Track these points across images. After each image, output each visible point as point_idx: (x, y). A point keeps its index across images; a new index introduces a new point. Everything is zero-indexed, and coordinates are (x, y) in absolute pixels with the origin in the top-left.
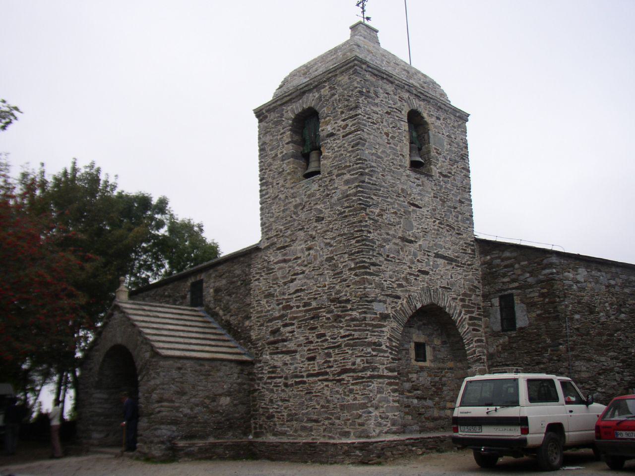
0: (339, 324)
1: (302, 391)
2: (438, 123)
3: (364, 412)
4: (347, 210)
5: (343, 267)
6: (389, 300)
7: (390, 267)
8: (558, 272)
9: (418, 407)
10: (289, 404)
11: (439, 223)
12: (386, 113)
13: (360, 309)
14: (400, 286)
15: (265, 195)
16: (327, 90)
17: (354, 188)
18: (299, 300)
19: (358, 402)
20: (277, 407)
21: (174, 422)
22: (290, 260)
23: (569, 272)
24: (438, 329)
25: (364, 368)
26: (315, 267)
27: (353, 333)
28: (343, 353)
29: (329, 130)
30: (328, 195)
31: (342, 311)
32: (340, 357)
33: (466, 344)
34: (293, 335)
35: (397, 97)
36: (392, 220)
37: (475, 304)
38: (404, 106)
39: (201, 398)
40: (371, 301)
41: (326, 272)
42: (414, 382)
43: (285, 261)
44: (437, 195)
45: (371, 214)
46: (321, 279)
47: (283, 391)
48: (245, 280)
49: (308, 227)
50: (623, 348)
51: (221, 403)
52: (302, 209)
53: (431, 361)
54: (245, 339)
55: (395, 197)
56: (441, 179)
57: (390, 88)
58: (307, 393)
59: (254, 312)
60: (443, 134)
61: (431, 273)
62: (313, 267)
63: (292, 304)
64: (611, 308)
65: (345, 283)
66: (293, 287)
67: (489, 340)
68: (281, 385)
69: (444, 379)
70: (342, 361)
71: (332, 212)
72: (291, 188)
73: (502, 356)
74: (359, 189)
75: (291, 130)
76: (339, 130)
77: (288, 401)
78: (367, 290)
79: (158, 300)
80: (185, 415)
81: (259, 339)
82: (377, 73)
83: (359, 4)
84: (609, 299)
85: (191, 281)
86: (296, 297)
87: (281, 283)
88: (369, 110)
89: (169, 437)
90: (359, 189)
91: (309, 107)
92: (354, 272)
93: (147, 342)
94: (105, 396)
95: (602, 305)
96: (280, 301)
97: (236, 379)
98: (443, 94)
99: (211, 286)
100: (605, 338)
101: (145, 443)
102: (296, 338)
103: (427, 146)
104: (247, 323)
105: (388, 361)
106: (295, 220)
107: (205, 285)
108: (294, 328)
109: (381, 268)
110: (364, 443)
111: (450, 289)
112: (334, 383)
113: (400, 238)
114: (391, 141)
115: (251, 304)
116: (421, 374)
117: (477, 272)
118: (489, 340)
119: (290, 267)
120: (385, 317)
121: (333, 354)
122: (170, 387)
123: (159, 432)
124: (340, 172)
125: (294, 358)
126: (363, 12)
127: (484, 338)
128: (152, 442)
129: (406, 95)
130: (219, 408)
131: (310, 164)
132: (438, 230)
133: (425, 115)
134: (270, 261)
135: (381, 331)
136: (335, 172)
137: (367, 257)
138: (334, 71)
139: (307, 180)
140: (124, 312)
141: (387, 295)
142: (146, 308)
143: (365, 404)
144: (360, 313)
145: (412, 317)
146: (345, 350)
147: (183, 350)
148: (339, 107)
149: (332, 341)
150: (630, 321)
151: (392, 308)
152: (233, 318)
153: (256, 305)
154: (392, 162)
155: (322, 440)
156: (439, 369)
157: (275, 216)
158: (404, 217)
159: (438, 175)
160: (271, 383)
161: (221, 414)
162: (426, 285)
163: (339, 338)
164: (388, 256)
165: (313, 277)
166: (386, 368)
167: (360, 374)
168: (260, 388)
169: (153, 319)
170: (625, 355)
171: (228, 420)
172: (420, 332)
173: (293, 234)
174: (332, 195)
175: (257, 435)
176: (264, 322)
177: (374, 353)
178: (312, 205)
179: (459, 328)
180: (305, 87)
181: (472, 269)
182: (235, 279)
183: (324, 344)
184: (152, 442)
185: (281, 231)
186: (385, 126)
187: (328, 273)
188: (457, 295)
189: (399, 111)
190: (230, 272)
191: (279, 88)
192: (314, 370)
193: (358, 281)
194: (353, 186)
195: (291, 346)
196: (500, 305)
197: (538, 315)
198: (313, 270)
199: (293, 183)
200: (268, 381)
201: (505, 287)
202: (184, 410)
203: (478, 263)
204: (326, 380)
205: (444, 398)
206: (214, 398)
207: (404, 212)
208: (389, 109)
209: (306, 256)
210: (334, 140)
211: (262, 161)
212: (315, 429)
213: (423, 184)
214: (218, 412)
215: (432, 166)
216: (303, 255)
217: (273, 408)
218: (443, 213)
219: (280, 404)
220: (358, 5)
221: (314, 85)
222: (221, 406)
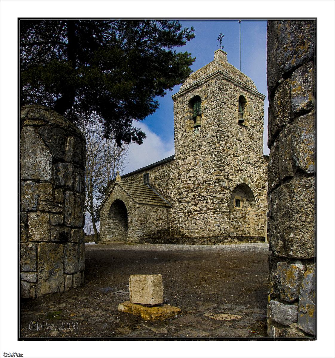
1: (191, 218)
3: (216, 225)
14: (232, 175)
19: (214, 221)
22: (187, 164)
25: (217, 208)
30: (204, 136)
41: (202, 169)
43: (185, 164)
45: (221, 144)
52: (193, 142)
57: (232, 86)
58: (193, 218)
60: (253, 107)
66: (188, 175)
69: (246, 215)
72: (188, 133)
75: (188, 106)
83: (219, 39)
111: (251, 177)
113: (232, 155)
116: (237, 212)
120: (225, 188)
126: (221, 43)
127: (264, 199)
129: (238, 89)
133: (246, 98)
145: (235, 188)
159: (250, 126)
167: (215, 210)
177: (221, 202)
194: (215, 132)
195: (187, 200)
220: (218, 40)
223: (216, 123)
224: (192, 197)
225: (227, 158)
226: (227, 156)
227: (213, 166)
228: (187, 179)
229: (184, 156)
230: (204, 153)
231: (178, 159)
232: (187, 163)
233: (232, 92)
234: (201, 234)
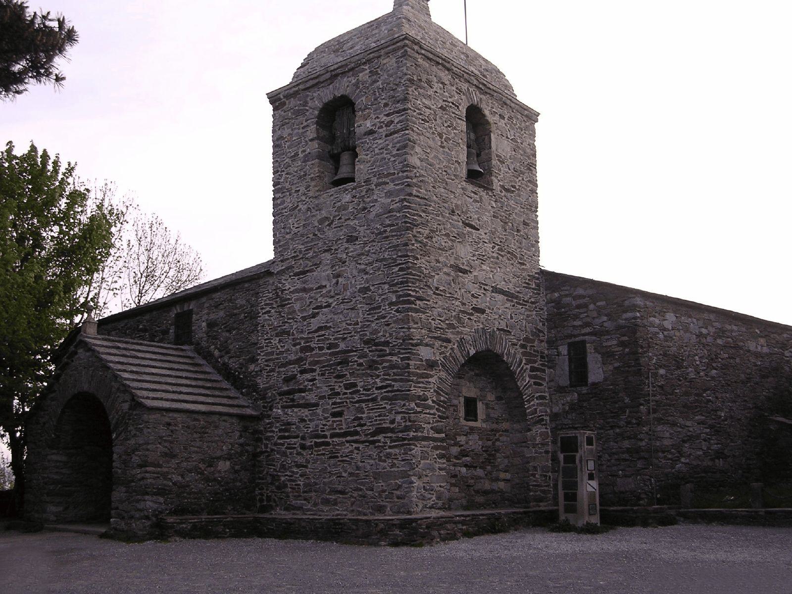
0: (374, 372)
1: (324, 454)
2: (502, 123)
4: (388, 229)
5: (382, 300)
6: (438, 343)
7: (440, 303)
8: (642, 316)
10: (307, 470)
11: (499, 250)
12: (440, 108)
13: (403, 354)
14: (451, 326)
15: (280, 205)
16: (366, 74)
18: (323, 340)
19: (396, 469)
20: (290, 474)
21: (161, 492)
23: (655, 317)
24: (492, 381)
26: (345, 299)
28: (379, 408)
29: (367, 126)
31: (379, 356)
33: (526, 401)
34: (314, 384)
35: (454, 88)
36: (443, 244)
37: (538, 352)
38: (462, 99)
40: (417, 345)
42: (462, 446)
43: (304, 290)
44: (497, 213)
46: (352, 314)
47: (298, 454)
49: (337, 247)
50: (712, 410)
51: (219, 468)
52: (329, 225)
53: (484, 421)
54: (248, 387)
55: (447, 215)
56: (503, 194)
57: (446, 77)
58: (331, 457)
59: (262, 354)
61: (488, 311)
62: (343, 300)
63: (313, 345)
64: (701, 362)
65: (384, 320)
66: (315, 323)
67: (553, 397)
69: (498, 443)
70: (378, 418)
71: (368, 231)
73: (569, 417)
74: (405, 203)
76: (382, 127)
77: (306, 467)
78: (411, 330)
79: (129, 335)
81: (270, 388)
82: (431, 56)
84: (699, 351)
85: (175, 312)
87: (299, 317)
88: (421, 103)
89: (155, 510)
90: (405, 203)
91: (342, 96)
93: (126, 389)
94: (64, 459)
95: (690, 358)
96: (298, 341)
98: (509, 87)
100: (692, 398)
101: (123, 518)
102: (318, 388)
104: (252, 367)
105: (434, 420)
106: (319, 239)
108: (315, 376)
110: (405, 519)
111: (508, 331)
112: (366, 445)
113: (451, 266)
115: (258, 343)
117: (541, 312)
118: (553, 397)
120: (431, 365)
121: (366, 410)
122: (157, 448)
123: (141, 506)
124: (380, 180)
125: (315, 413)
127: (546, 394)
128: (132, 517)
129: (464, 86)
130: (217, 475)
131: (340, 168)
132: (498, 258)
133: (487, 112)
134: (285, 290)
135: (427, 382)
136: (375, 180)
137: (413, 289)
138: (377, 51)
139: (336, 188)
140: (94, 351)
141: (435, 338)
142: (119, 345)
143: (406, 471)
144: (402, 359)
146: (382, 405)
147: (173, 400)
148: (383, 97)
149: (364, 392)
150: (721, 379)
151: (440, 354)
152: (232, 360)
154: (445, 171)
155: (350, 516)
156: (492, 430)
157: (293, 233)
158: (457, 240)
160: (283, 445)
161: (219, 483)
162: (481, 326)
163: (374, 389)
165: (342, 312)
166: (432, 428)
167: (400, 435)
168: (269, 450)
169: (131, 361)
170: (714, 419)
171: (227, 490)
172: (472, 384)
173: (316, 256)
174: (369, 209)
175: (264, 509)
176: (275, 367)
177: (419, 409)
178: (343, 220)
179: (518, 381)
180: (338, 68)
181: (536, 307)
183: (355, 396)
184: (132, 517)
185: (300, 252)
186: (438, 125)
187: (362, 307)
188: (517, 340)
189: (456, 106)
190: (230, 301)
191: (301, 67)
192: (340, 429)
193: (400, 319)
194: (397, 199)
195: (311, 398)
196: (569, 354)
197: (615, 368)
198: (341, 303)
199: (317, 191)
200: (279, 441)
201: (576, 332)
203: (544, 300)
204: (356, 442)
205: (498, 466)
206: (211, 462)
208: (444, 103)
209: (334, 285)
210: (374, 139)
211: (277, 161)
212: (340, 503)
213: (481, 199)
214: (215, 480)
216: (329, 284)
218: (504, 237)
219: (295, 470)
221: (349, 67)
222: (219, 472)
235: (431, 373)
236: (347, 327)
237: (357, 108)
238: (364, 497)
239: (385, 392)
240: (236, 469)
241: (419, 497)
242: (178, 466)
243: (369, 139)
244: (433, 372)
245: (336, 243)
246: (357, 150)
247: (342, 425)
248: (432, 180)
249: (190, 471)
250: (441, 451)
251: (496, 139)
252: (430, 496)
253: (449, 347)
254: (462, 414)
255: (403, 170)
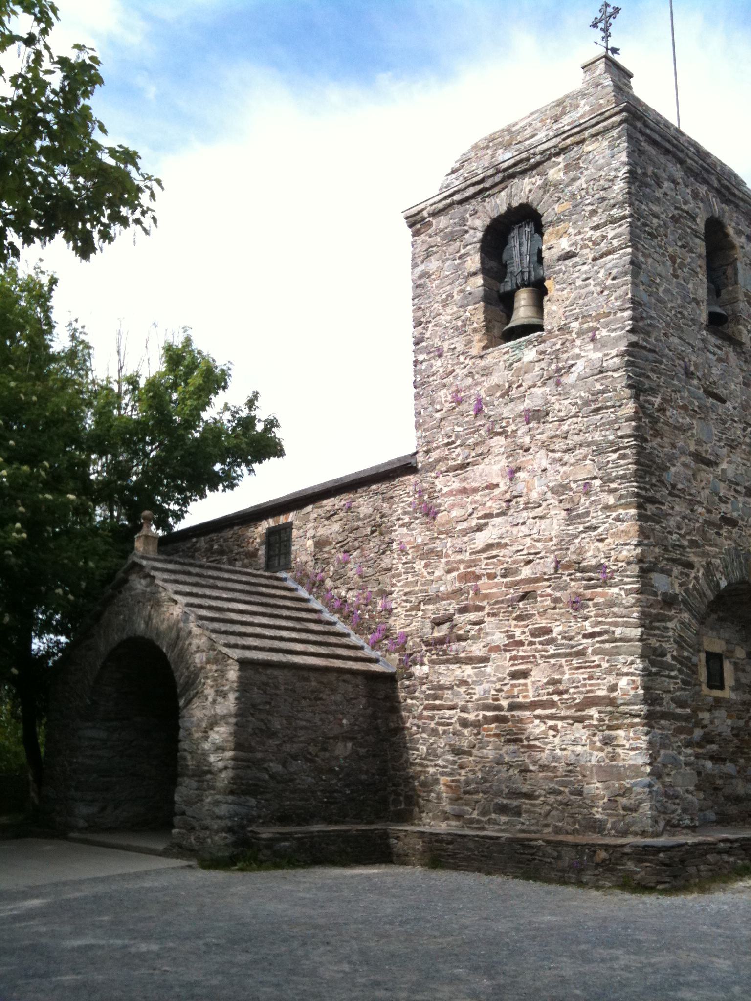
6: (676, 570)
9: (714, 776)
10: (471, 758)
14: (693, 544)
17: (617, 356)
22: (475, 490)
27: (613, 628)
32: (583, 673)
34: (480, 629)
35: (689, 191)
36: (680, 420)
39: (301, 742)
43: (464, 491)
48: (380, 526)
51: (337, 752)
53: (734, 689)
59: (399, 584)
61: (741, 523)
62: (526, 504)
63: (478, 571)
66: (481, 539)
68: (452, 721)
70: (587, 682)
76: (586, 247)
80: (272, 777)
86: (488, 558)
92: (614, 514)
96: (455, 565)
97: (364, 709)
99: (308, 535)
103: (731, 289)
107: (295, 533)
109: (663, 508)
112: (568, 724)
113: (691, 454)
114: (679, 272)
116: (717, 713)
119: (475, 502)
129: (703, 189)
133: (731, 231)
149: (564, 641)
152: (351, 593)
153: (403, 571)
154: (679, 313)
157: (445, 410)
158: (698, 416)
160: (432, 718)
161: (337, 774)
163: (581, 637)
164: (674, 486)
166: (672, 699)
171: (347, 786)
173: (483, 442)
182: (360, 524)
192: (524, 697)
193: (622, 532)
195: (477, 649)
198: (524, 509)
202: (271, 765)
204: (552, 717)
207: (699, 407)
212: (526, 812)
215: (740, 327)
217: (436, 765)
220: (595, 25)
221: (532, 161)
222: (337, 758)
223: (619, 314)
224: (499, 639)
225: (673, 469)
226: (672, 459)
227: (611, 500)
228: (473, 557)
229: (459, 455)
230: (559, 445)
231: (432, 466)
232: (475, 485)
233: (679, 197)
234: (549, 820)
235: (670, 614)
236: (534, 543)
237: (544, 220)
238: (566, 804)
239: (598, 642)
240: (361, 754)
241: (660, 809)
242: (279, 750)
243: (566, 266)
244: (673, 612)
245: (514, 421)
246: (547, 284)
247: (527, 691)
248: (664, 324)
249: (295, 757)
250: (686, 736)
251: (744, 270)
252: (674, 807)
253: (693, 575)
254: (703, 676)
255: (623, 307)
